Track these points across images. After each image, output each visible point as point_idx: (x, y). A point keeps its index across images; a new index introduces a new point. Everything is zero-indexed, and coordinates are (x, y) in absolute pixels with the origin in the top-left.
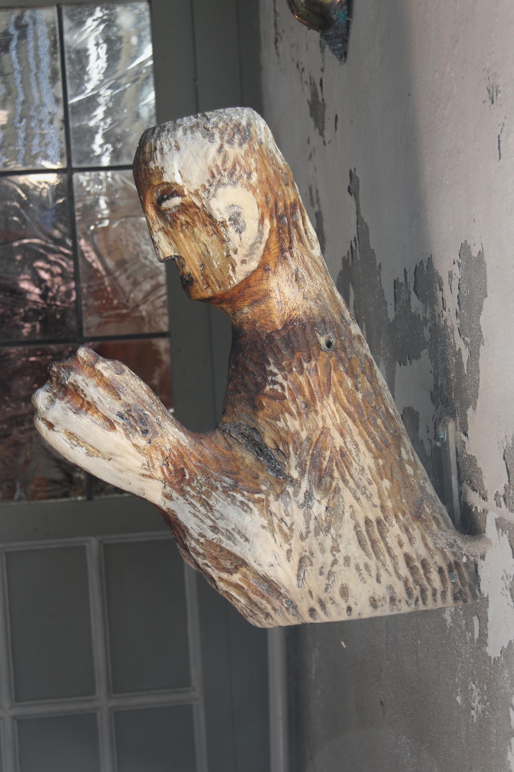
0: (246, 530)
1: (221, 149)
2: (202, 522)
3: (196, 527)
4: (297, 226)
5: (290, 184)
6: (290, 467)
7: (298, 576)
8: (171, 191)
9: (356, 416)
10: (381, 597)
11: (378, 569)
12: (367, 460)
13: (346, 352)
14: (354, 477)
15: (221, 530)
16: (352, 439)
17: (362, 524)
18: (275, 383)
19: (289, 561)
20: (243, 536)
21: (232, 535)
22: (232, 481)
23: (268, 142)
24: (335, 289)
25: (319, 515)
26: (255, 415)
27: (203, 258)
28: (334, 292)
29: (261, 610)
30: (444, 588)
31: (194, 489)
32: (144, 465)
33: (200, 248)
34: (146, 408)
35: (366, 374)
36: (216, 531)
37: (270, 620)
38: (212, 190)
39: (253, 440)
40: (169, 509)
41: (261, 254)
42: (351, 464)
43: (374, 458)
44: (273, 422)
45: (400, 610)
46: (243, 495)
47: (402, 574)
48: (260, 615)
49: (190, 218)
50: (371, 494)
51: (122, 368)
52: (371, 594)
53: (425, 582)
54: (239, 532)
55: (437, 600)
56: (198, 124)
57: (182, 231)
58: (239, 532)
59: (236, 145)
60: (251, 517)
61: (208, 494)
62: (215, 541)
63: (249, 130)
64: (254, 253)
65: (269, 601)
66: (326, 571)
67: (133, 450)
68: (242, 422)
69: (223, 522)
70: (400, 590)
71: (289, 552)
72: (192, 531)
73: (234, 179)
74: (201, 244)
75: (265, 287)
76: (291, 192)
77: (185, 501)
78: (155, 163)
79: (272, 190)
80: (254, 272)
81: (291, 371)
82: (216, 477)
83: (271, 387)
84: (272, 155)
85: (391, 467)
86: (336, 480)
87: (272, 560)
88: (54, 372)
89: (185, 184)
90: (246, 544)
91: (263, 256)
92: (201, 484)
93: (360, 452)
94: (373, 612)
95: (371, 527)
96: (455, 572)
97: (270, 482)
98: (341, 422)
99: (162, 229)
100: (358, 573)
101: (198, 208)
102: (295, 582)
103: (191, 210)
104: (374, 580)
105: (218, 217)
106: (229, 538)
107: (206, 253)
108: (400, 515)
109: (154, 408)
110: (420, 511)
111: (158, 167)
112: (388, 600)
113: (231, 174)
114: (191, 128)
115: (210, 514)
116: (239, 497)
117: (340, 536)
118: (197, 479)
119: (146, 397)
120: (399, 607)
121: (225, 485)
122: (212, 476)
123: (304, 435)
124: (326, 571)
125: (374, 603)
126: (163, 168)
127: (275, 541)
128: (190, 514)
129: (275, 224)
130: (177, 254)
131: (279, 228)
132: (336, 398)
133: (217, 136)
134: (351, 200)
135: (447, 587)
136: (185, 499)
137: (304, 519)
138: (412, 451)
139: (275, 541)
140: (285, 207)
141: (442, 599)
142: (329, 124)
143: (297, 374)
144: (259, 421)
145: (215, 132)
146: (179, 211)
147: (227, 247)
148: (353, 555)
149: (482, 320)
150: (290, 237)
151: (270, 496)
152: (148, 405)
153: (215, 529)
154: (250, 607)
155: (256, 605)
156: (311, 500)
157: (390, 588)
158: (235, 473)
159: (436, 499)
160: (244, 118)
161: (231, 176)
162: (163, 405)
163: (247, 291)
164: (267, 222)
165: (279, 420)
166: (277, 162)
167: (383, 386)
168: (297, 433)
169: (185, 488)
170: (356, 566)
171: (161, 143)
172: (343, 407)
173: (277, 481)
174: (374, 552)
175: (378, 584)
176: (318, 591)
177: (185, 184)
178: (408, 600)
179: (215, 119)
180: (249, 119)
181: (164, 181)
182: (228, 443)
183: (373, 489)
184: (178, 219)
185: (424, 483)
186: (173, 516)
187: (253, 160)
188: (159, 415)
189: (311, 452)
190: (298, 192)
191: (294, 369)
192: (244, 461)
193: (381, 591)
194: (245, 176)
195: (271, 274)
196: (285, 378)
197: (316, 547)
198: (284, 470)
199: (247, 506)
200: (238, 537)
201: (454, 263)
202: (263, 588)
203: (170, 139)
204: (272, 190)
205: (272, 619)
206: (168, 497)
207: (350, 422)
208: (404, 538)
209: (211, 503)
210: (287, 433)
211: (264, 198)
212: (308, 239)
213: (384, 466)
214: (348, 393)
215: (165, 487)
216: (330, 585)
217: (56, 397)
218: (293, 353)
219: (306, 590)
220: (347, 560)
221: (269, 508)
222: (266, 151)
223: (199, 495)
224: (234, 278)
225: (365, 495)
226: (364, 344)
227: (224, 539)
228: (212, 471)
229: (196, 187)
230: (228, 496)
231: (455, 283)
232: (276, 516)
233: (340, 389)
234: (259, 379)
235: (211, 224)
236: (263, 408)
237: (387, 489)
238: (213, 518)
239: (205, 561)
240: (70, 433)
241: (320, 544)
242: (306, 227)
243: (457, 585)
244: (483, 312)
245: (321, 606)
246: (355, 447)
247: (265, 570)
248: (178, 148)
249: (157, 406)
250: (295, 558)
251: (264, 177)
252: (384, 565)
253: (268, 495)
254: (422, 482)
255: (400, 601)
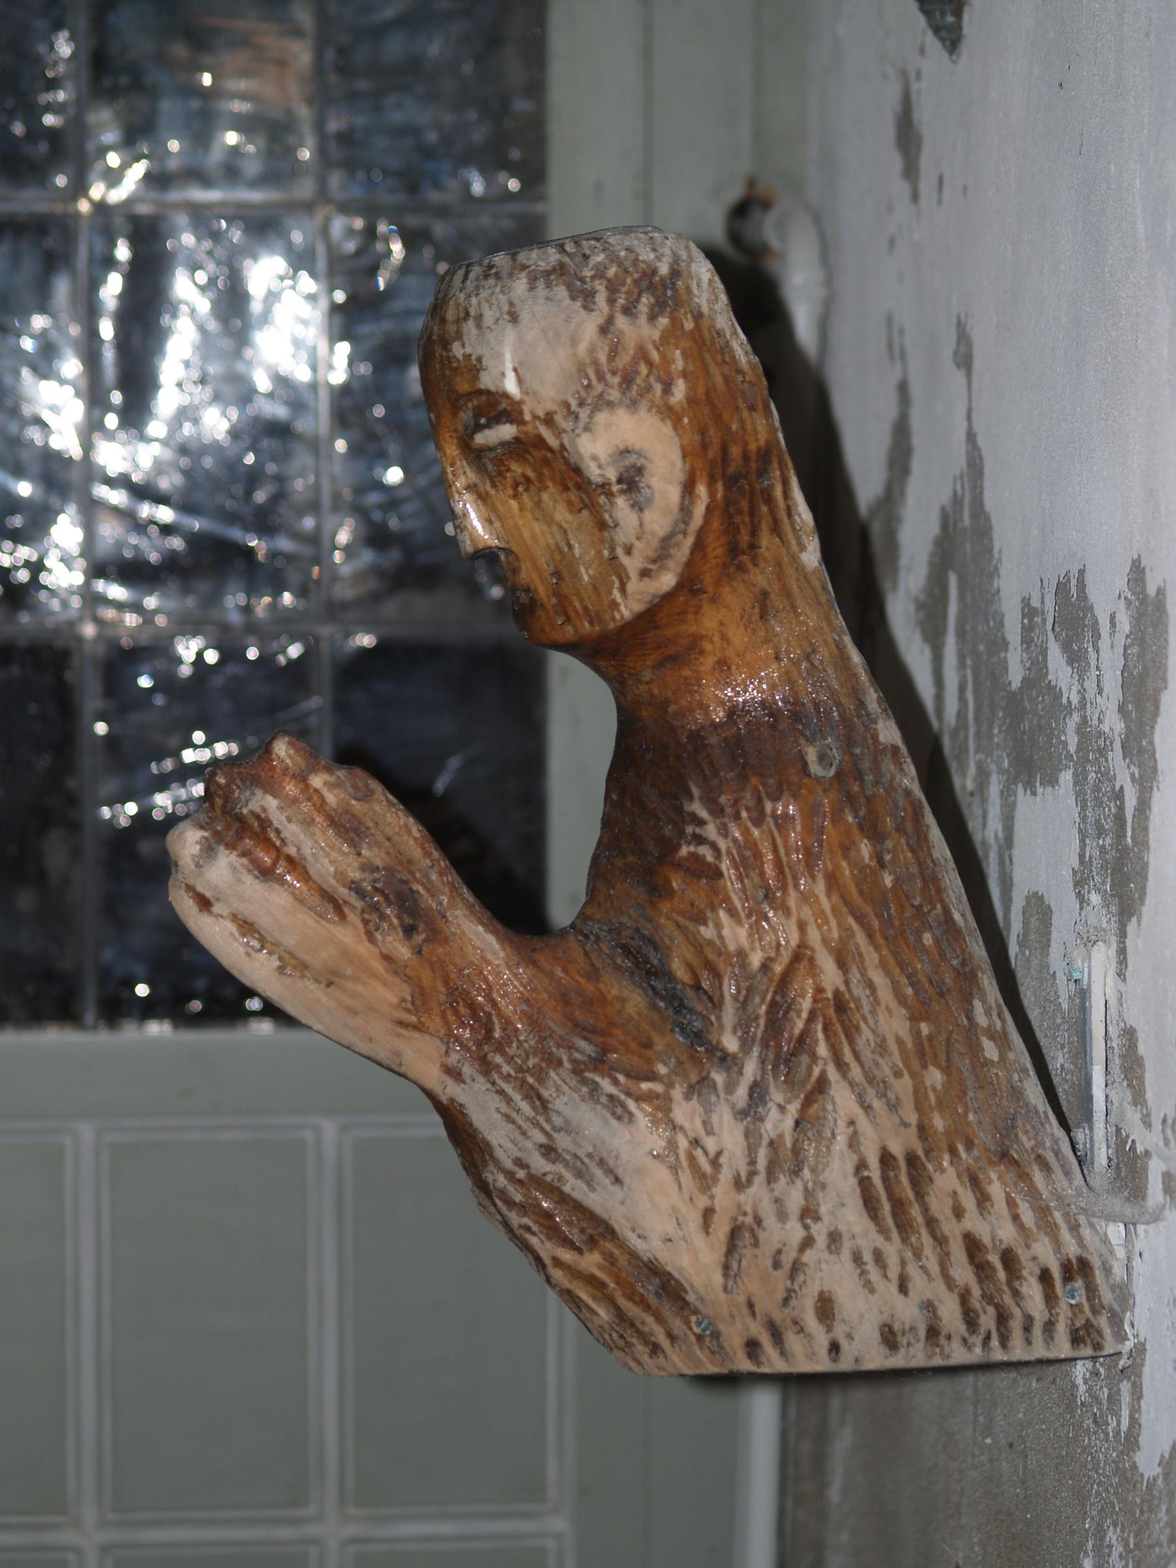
0: (617, 1158)
1: (604, 330)
2: (524, 1133)
3: (510, 1146)
4: (769, 500)
5: (760, 407)
6: (721, 1027)
7: (726, 1268)
8: (496, 408)
9: (876, 924)
10: (907, 1327)
11: (903, 1263)
12: (893, 1023)
13: (862, 781)
14: (863, 1059)
15: (564, 1155)
16: (862, 975)
17: (874, 1162)
18: (699, 840)
19: (708, 1233)
20: (609, 1171)
21: (587, 1168)
22: (594, 1048)
23: (715, 312)
24: (847, 640)
25: (781, 1136)
26: (653, 905)
27: (558, 557)
28: (845, 647)
29: (644, 1337)
30: (1051, 1315)
31: (510, 1060)
32: (403, 1000)
33: (553, 537)
34: (414, 877)
35: (905, 833)
36: (553, 1155)
37: (662, 1359)
38: (584, 414)
39: (647, 962)
40: (452, 1100)
41: (685, 559)
42: (858, 1029)
43: (910, 1019)
44: (691, 926)
45: (948, 1356)
46: (616, 1082)
47: (957, 1277)
48: (640, 1348)
49: (534, 470)
50: (897, 1098)
51: (367, 786)
52: (885, 1318)
53: (1007, 1299)
54: (602, 1163)
55: (1034, 1341)
56: (562, 265)
57: (515, 496)
58: (602, 1163)
59: (643, 319)
60: (630, 1133)
61: (542, 1078)
62: (549, 1178)
63: (674, 284)
64: (668, 556)
65: (659, 1319)
66: (787, 1260)
67: (379, 967)
68: (624, 919)
69: (569, 1139)
70: (950, 1313)
71: (708, 1213)
72: (499, 1154)
73: (634, 393)
74: (555, 528)
75: (693, 629)
76: (760, 423)
77: (489, 1086)
78: (463, 346)
79: (718, 419)
80: (668, 596)
81: (737, 817)
82: (560, 1037)
83: (692, 849)
84: (722, 342)
85: (948, 1040)
86: (820, 1062)
87: (670, 1228)
88: (219, 785)
89: (525, 398)
90: (615, 1188)
91: (689, 564)
92: (525, 1051)
93: (878, 1003)
94: (886, 1357)
95: (893, 1170)
96: (1079, 1284)
97: (677, 1058)
98: (840, 937)
99: (470, 488)
100: (859, 1271)
101: (550, 450)
102: (718, 1278)
103: (538, 454)
104: (894, 1288)
105: (594, 472)
106: (579, 1175)
107: (566, 549)
108: (961, 1148)
109: (434, 877)
110: (1007, 1143)
111: (470, 355)
112: (922, 1333)
113: (627, 381)
114: (547, 274)
115: (541, 1119)
116: (606, 1085)
117: (823, 1186)
118: (518, 1040)
119: (416, 852)
120: (947, 1350)
121: (578, 1056)
122: (551, 1036)
123: (756, 960)
124: (787, 1260)
125: (890, 1337)
126: (479, 359)
127: (680, 1187)
128: (499, 1116)
129: (719, 495)
130: (503, 545)
131: (728, 502)
132: (832, 881)
133: (601, 299)
134: (959, 376)
135: (1058, 1314)
136: (489, 1081)
137: (745, 1144)
138: (998, 1006)
139: (680, 1187)
140: (746, 456)
141: (1045, 1340)
142: (926, 186)
143: (749, 824)
144: (662, 921)
145: (598, 287)
146: (510, 453)
147: (612, 539)
148: (849, 1230)
149: (1157, 738)
150: (752, 522)
151: (674, 1087)
152: (420, 871)
153: (549, 1151)
154: (618, 1329)
155: (632, 1325)
156: (765, 1104)
157: (929, 1307)
158: (602, 1033)
159: (1047, 1117)
160: (664, 259)
161: (628, 388)
162: (454, 872)
163: (651, 635)
164: (702, 490)
165: (705, 923)
166: (733, 357)
167: (942, 861)
168: (742, 954)
169: (490, 1056)
170: (854, 1254)
171: (479, 304)
172: (847, 903)
173: (692, 1057)
174: (898, 1225)
175: (902, 1297)
176: (768, 1304)
177: (525, 398)
178: (966, 1335)
179: (600, 258)
180: (676, 259)
181: (482, 386)
182: (593, 965)
183: (903, 1087)
184: (509, 470)
185: (1021, 1081)
186: (461, 1118)
187: (678, 352)
188: (443, 894)
189: (769, 997)
190: (777, 424)
191: (744, 814)
192: (623, 1007)
193: (907, 1312)
194: (658, 388)
195: (705, 605)
196: (724, 832)
197: (767, 1209)
198: (709, 1032)
199: (623, 1106)
200: (598, 1173)
201: (1119, 597)
202: (648, 1289)
203: (501, 296)
204: (718, 419)
205: (666, 1357)
206: (454, 1074)
207: (860, 937)
208: (968, 1200)
209: (545, 1093)
210: (721, 951)
211: (697, 437)
212: (794, 529)
213: (931, 1038)
214: (860, 871)
215: (447, 1052)
216: (795, 1291)
217: (219, 842)
218: (744, 778)
219: (742, 1299)
220: (834, 1238)
221: (671, 1115)
222: (710, 332)
223: (520, 1075)
224: (622, 608)
225: (884, 1100)
226: (905, 766)
227: (568, 1175)
228: (552, 1024)
229: (550, 406)
230: (584, 1081)
231: (1120, 640)
232: (685, 1134)
233: (844, 864)
234: (668, 830)
235: (579, 487)
236: (671, 893)
237: (934, 1090)
238: (548, 1128)
239: (526, 1221)
240: (245, 922)
241: (777, 1201)
242: (790, 503)
243: (1082, 1311)
244: (1159, 720)
245: (773, 1335)
246: (868, 992)
247: (650, 1247)
248: (514, 318)
249: (441, 873)
250: (721, 1228)
251: (701, 390)
252: (918, 1255)
253: (670, 1085)
254: (1016, 1077)
255: (949, 1337)
